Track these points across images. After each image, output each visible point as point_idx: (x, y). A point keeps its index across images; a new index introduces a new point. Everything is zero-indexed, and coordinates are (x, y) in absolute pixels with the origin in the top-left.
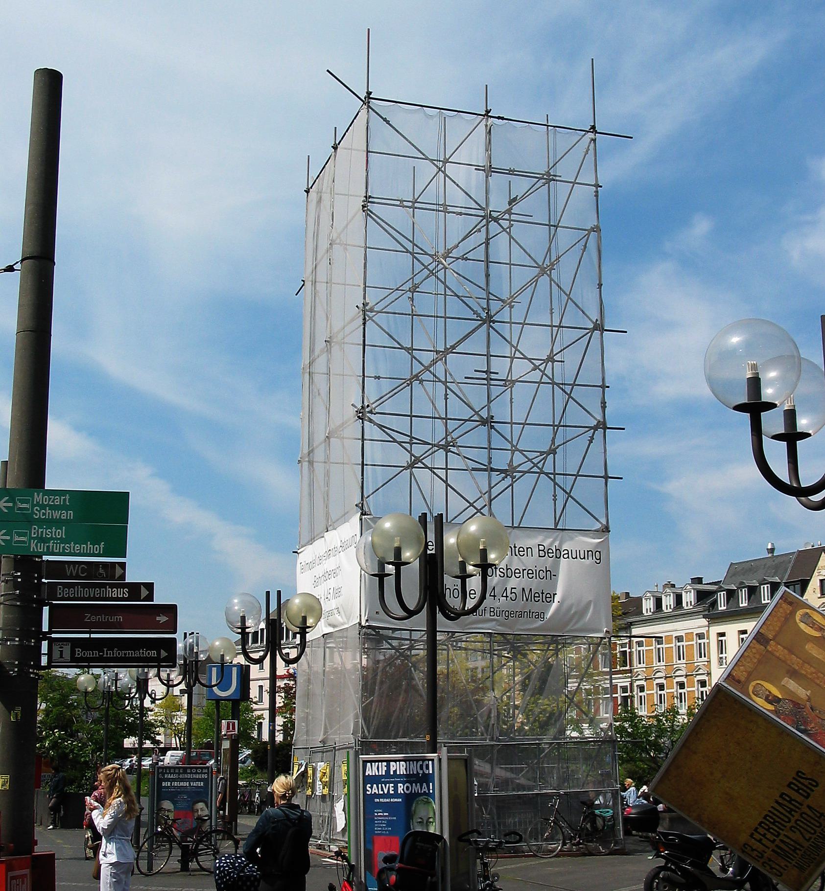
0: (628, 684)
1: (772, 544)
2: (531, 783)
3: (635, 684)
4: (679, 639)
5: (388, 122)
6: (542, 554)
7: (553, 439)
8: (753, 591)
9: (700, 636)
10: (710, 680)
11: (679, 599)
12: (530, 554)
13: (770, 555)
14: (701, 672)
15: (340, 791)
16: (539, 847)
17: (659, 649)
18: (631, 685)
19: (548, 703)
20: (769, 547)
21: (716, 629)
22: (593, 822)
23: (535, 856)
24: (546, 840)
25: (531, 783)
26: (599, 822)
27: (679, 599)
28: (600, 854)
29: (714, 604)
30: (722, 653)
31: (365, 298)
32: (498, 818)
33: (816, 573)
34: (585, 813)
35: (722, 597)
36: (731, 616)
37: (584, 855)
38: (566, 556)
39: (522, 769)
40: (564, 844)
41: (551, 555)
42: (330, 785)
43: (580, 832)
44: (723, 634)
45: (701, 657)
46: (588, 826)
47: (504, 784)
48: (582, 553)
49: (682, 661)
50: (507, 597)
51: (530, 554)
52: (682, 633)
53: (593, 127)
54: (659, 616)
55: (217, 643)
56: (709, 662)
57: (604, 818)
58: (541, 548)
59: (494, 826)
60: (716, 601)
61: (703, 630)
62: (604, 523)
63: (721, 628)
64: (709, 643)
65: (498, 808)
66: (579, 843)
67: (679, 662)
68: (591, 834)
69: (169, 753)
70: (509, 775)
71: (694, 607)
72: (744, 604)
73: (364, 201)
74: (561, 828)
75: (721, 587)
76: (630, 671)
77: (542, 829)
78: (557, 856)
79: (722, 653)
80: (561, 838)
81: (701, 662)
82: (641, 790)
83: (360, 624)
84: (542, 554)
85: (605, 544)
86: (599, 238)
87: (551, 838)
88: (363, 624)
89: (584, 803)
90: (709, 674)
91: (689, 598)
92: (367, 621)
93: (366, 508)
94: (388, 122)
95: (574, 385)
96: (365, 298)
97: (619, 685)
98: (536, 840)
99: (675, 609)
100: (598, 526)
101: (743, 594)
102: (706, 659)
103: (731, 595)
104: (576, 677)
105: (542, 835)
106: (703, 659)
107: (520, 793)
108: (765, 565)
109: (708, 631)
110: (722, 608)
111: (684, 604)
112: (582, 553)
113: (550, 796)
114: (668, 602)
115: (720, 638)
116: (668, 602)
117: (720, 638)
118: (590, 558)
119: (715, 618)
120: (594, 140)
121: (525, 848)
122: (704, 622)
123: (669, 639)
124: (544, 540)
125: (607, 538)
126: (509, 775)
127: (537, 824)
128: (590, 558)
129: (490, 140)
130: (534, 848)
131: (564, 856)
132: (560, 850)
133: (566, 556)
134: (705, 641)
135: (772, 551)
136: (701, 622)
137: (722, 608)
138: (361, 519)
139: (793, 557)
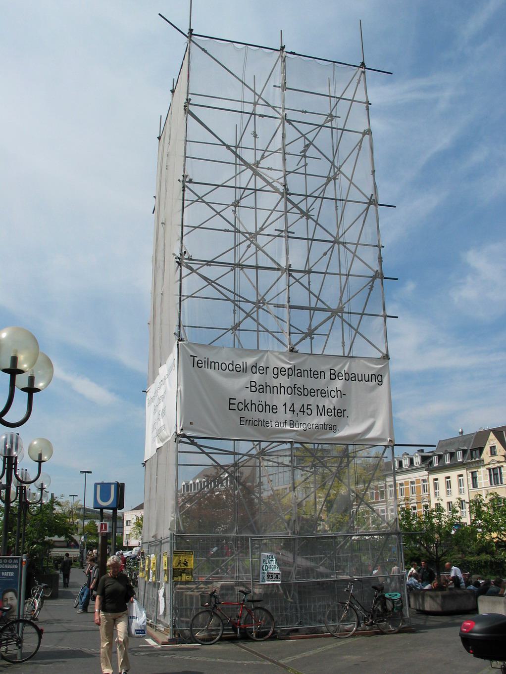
0: (385, 508)
1: (462, 429)
2: (328, 571)
3: (389, 508)
4: (412, 483)
5: (206, 52)
6: (333, 377)
7: (341, 298)
8: (452, 455)
9: (424, 481)
10: (430, 504)
11: (411, 461)
12: (323, 377)
13: (461, 435)
14: (425, 500)
15: (163, 579)
16: (337, 629)
17: (401, 489)
18: (387, 509)
19: (341, 517)
20: (460, 431)
21: (432, 477)
22: (384, 605)
23: (332, 636)
24: (342, 621)
25: (328, 571)
26: (389, 605)
27: (411, 461)
28: (390, 632)
29: (431, 463)
30: (436, 489)
31: (184, 171)
32: (300, 603)
33: (487, 443)
34: (376, 596)
35: (435, 459)
36: (440, 469)
37: (377, 633)
38: (353, 379)
39: (321, 559)
40: (359, 625)
41: (340, 378)
42: (157, 574)
43: (373, 614)
44: (436, 479)
45: (425, 492)
46: (380, 608)
47: (307, 572)
48: (367, 376)
49: (414, 495)
50: (304, 412)
51: (323, 377)
52: (414, 480)
53: (363, 64)
54: (401, 470)
55: (35, 443)
56: (429, 495)
57: (393, 601)
58: (333, 372)
59: (296, 609)
60: (432, 461)
61: (426, 478)
62: (385, 352)
63: (435, 476)
64: (429, 484)
65: (299, 593)
66: (372, 624)
67: (413, 495)
68: (381, 614)
69: (135, 549)
70: (312, 564)
71: (420, 465)
72: (448, 462)
73: (185, 103)
74: (355, 610)
75: (435, 453)
76: (386, 501)
77: (339, 611)
78: (354, 635)
79: (436, 489)
80: (356, 620)
81: (425, 495)
82: (410, 571)
83: (176, 432)
84: (333, 377)
85: (386, 367)
86: (371, 139)
87: (347, 620)
88: (179, 433)
89: (375, 588)
90: (429, 501)
91: (417, 460)
92: (182, 430)
93: (183, 336)
94: (206, 52)
95: (357, 244)
96: (184, 171)
97: (380, 509)
98: (334, 620)
99: (409, 467)
100: (380, 355)
101: (447, 456)
102: (427, 493)
103: (440, 457)
104: (356, 505)
105: (339, 618)
106: (426, 493)
107: (319, 580)
108: (458, 441)
109: (428, 478)
110: (436, 465)
111: (415, 464)
112: (367, 376)
113: (346, 581)
114: (406, 463)
115: (435, 482)
116: (406, 463)
117: (435, 482)
118: (374, 381)
119: (431, 470)
120: (364, 72)
121: (324, 629)
122: (426, 473)
123: (407, 483)
124: (336, 365)
125: (388, 364)
126: (312, 564)
127: (334, 607)
128: (374, 381)
129: (284, 66)
130: (332, 628)
131: (359, 635)
132: (356, 630)
133: (353, 379)
134: (427, 483)
135: (462, 433)
136: (423, 474)
137: (436, 465)
138: (178, 345)
139: (474, 436)
